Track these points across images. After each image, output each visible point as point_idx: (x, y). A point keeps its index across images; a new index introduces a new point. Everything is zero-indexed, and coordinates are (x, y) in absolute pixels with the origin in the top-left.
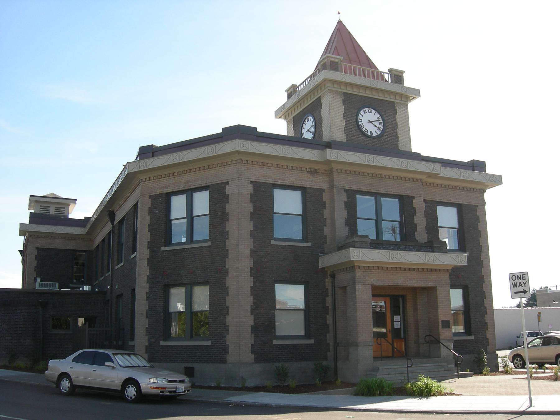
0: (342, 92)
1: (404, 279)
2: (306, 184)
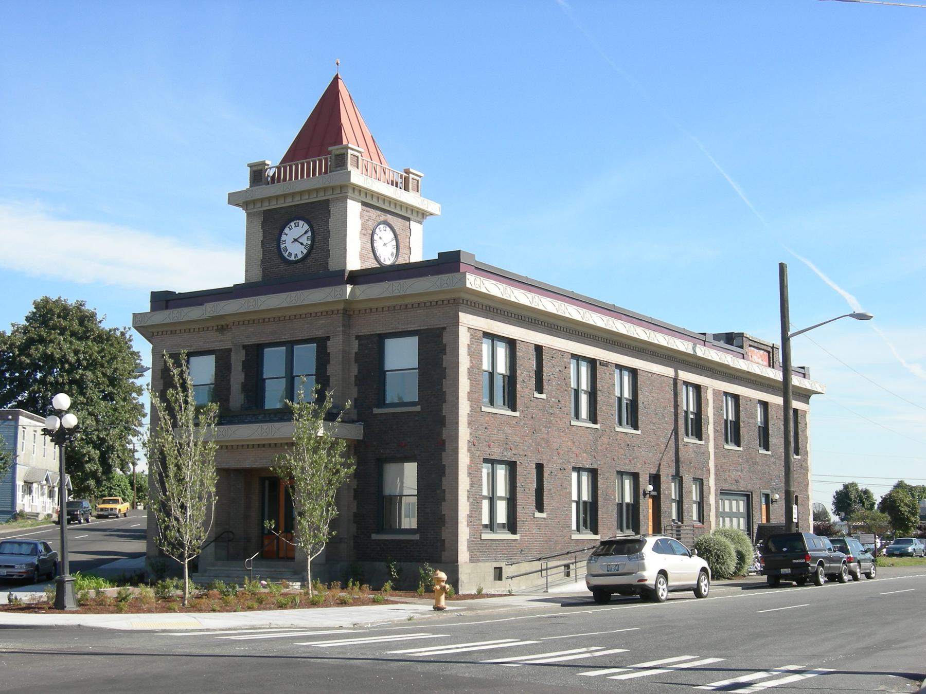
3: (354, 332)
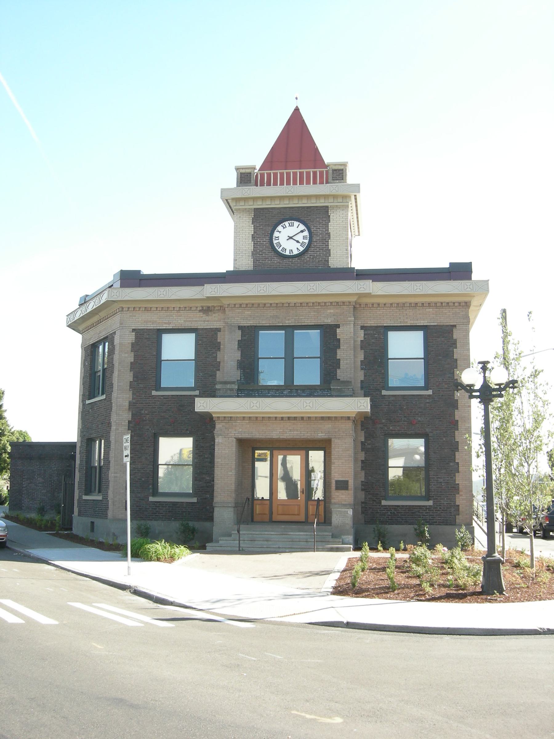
0: (252, 208)
1: (281, 430)
2: (197, 325)
3: (360, 323)
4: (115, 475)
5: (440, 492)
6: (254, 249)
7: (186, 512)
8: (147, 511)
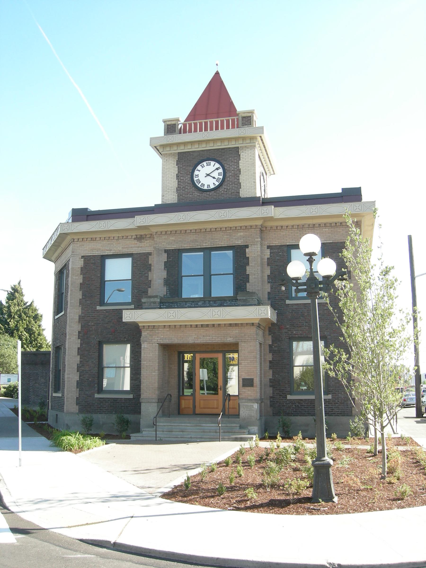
2: (132, 251)
4: (69, 376)
5: (338, 387)
6: (178, 186)
7: (124, 406)
8: (93, 406)
